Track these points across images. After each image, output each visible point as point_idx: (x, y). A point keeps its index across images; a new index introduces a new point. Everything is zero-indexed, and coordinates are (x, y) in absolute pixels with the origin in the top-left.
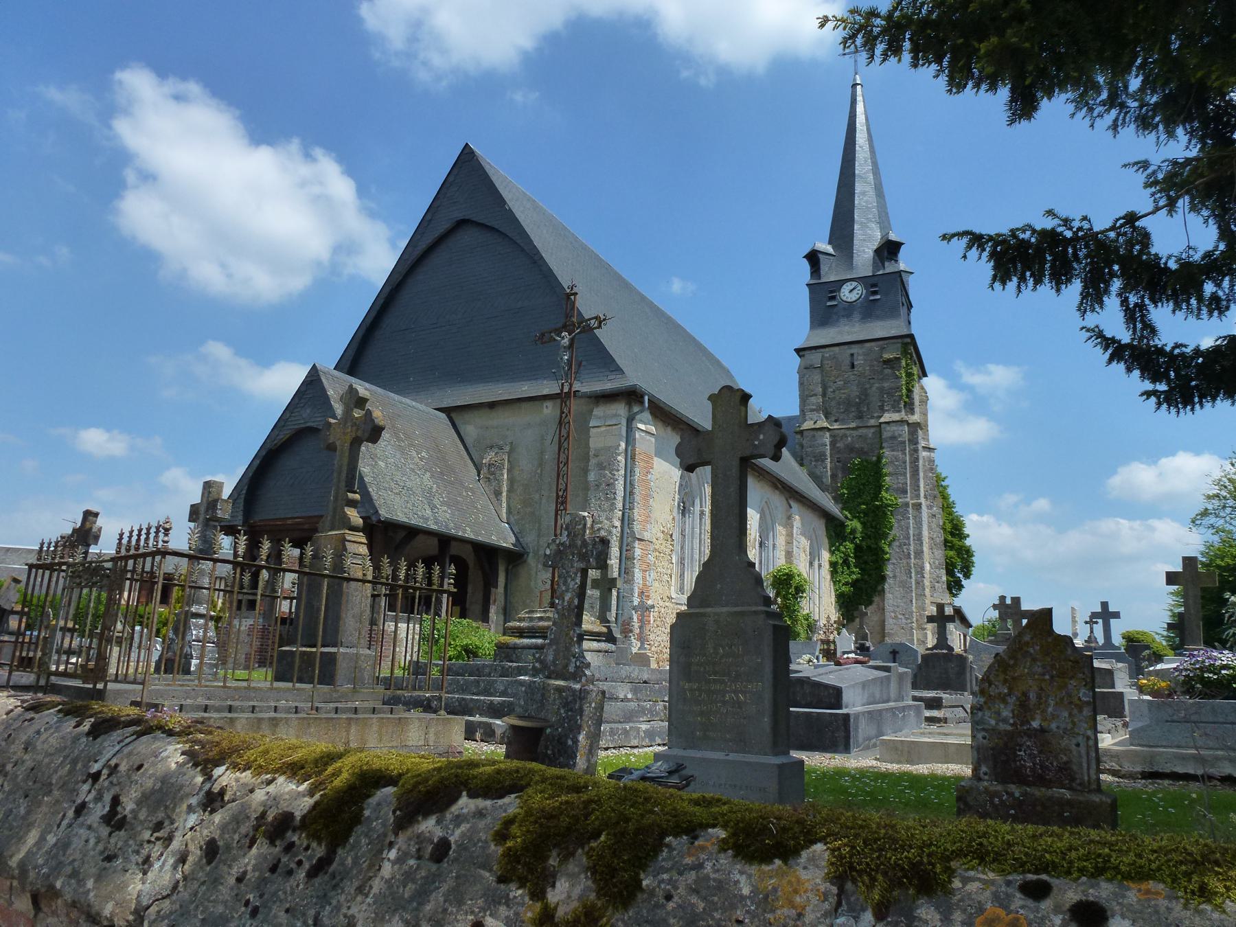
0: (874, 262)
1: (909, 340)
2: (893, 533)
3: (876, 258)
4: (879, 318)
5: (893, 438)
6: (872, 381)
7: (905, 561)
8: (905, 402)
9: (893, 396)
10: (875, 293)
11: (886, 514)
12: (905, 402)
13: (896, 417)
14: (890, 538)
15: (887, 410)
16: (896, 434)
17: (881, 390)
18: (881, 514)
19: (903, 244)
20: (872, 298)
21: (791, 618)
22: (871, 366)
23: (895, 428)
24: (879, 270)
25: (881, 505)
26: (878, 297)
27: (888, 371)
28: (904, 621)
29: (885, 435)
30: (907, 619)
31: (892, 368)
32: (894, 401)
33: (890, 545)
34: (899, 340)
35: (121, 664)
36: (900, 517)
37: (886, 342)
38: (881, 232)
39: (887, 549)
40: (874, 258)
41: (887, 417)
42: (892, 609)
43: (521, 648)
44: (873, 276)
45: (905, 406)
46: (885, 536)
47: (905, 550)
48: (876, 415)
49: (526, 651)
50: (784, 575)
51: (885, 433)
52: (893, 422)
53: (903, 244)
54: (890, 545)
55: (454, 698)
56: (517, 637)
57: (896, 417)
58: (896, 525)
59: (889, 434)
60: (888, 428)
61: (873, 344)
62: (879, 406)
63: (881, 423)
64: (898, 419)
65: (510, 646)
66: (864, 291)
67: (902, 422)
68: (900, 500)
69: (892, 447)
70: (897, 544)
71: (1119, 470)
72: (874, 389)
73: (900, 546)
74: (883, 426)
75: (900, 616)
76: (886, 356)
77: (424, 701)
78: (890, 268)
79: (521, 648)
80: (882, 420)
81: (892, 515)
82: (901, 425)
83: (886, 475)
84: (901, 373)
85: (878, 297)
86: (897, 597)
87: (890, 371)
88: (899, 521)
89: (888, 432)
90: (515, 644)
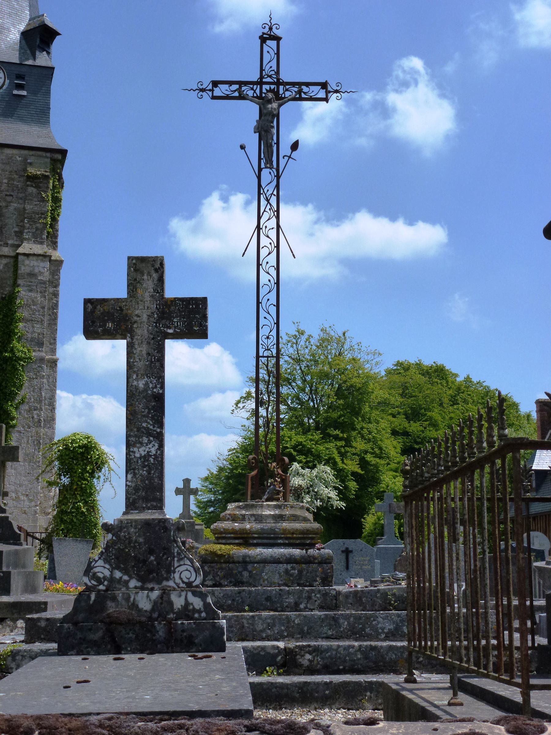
0: (21, 48)
1: (59, 157)
2: (22, 393)
3: (24, 42)
4: (22, 120)
5: (32, 275)
6: (9, 199)
7: (34, 430)
8: (48, 233)
9: (35, 222)
10: (20, 87)
11: (17, 369)
12: (48, 233)
13: (38, 249)
14: (18, 399)
15: (26, 239)
16: (36, 270)
17: (22, 213)
18: (9, 368)
19: (59, 34)
20: (15, 92)
21: (86, 503)
22: (10, 179)
23: (36, 263)
24: (27, 59)
25: (10, 358)
26: (24, 93)
27: (32, 190)
28: (27, 503)
29: (23, 269)
30: (31, 501)
31: (37, 187)
32: (37, 229)
33: (17, 408)
34: (48, 155)
35: (475, 624)
36: (31, 374)
37: (31, 153)
38: (30, 11)
39: (14, 413)
40: (20, 41)
41: (26, 248)
42: (13, 488)
43: (258, 562)
44: (20, 64)
45: (47, 237)
46: (12, 396)
47: (35, 416)
48: (10, 242)
49: (269, 567)
50: (80, 447)
51: (23, 268)
52: (34, 255)
53: (59, 34)
54: (17, 408)
55: (353, 647)
56: (239, 545)
57: (38, 249)
58: (26, 384)
59: (28, 270)
60: (27, 262)
61: (15, 151)
62: (15, 232)
63: (18, 254)
64: (40, 252)
65: (236, 559)
66: (7, 82)
67: (44, 256)
68: (34, 354)
69: (29, 286)
70: (26, 407)
71: (73, 339)
72: (11, 208)
73: (29, 411)
74: (20, 258)
75: (22, 498)
76: (32, 170)
77: (277, 655)
78: (42, 60)
79: (258, 562)
80: (20, 250)
81: (23, 371)
82: (42, 261)
83: (20, 320)
84: (48, 196)
85: (24, 93)
86: (21, 474)
87: (34, 190)
88: (31, 379)
89: (25, 266)
90: (245, 556)
